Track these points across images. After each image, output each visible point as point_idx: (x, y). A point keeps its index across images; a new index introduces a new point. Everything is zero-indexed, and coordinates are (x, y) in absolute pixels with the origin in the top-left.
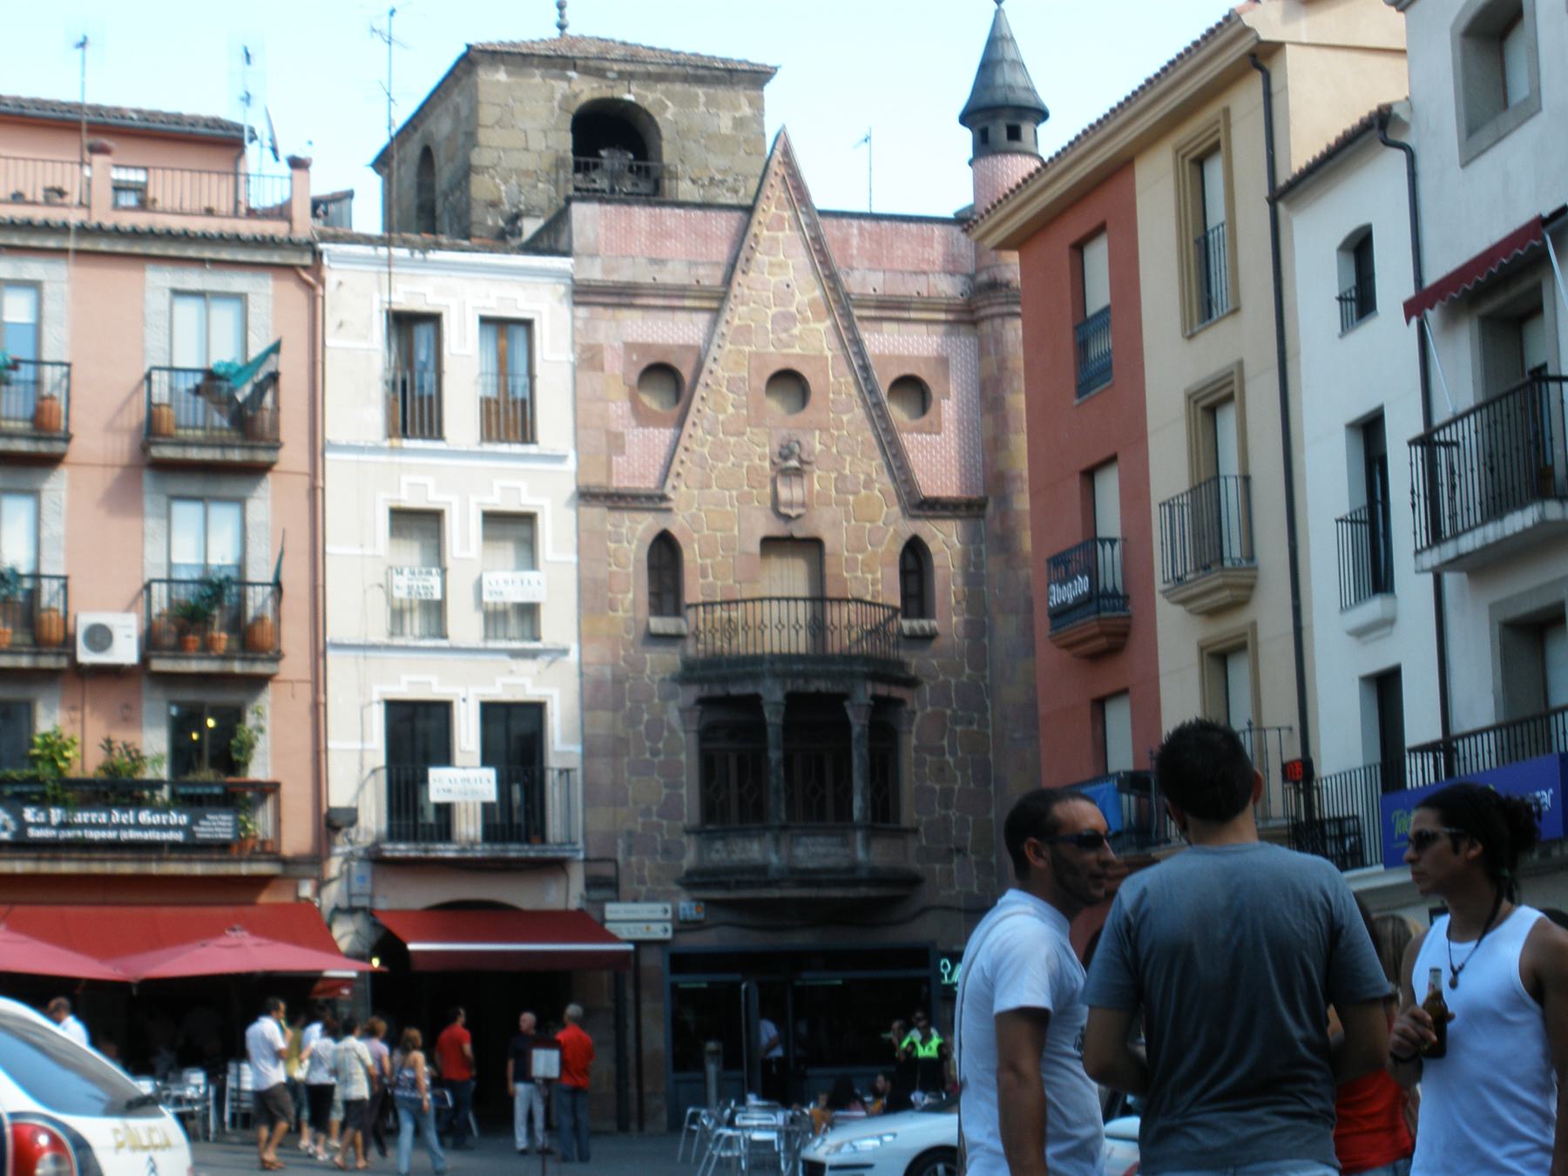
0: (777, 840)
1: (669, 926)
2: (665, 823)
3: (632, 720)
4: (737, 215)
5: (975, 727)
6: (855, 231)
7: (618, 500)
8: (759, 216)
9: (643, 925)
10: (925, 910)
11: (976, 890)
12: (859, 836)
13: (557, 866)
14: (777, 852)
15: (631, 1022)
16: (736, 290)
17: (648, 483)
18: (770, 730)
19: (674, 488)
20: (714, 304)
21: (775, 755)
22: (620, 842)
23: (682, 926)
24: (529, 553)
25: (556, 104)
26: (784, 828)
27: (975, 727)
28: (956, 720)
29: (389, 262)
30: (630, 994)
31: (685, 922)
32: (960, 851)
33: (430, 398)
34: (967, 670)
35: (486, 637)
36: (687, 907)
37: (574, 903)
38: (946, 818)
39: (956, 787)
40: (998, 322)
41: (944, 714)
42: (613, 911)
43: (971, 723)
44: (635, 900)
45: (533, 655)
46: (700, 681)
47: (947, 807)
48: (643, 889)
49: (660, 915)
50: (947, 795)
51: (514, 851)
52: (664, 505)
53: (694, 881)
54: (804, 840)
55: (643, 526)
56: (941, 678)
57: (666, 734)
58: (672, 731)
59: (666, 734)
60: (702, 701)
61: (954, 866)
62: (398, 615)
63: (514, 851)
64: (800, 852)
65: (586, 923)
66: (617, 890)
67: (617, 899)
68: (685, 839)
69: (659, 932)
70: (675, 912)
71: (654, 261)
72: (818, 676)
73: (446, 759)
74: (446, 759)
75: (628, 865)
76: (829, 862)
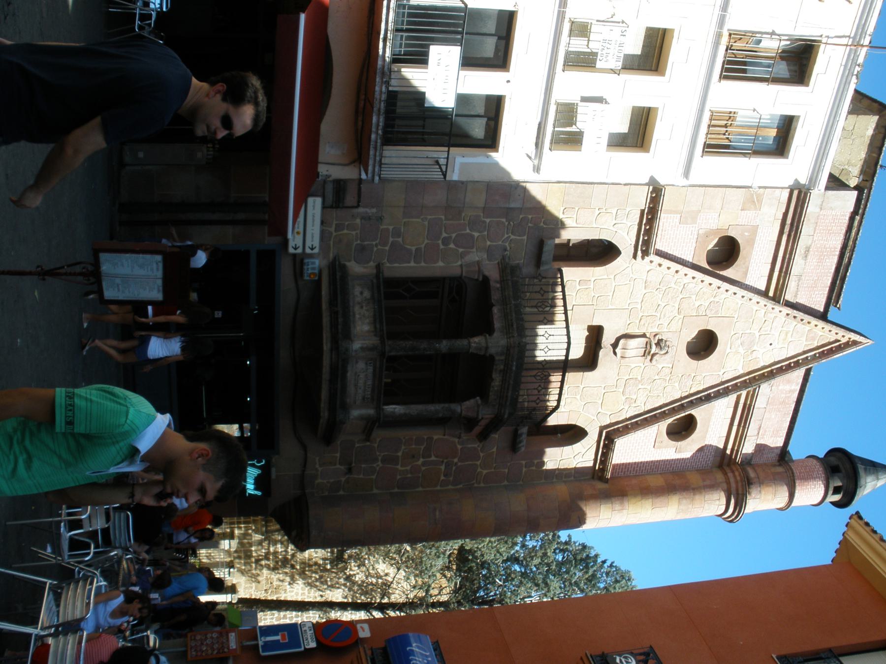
0: (372, 349)
1: (300, 251)
2: (387, 248)
6: (793, 388)
7: (650, 217)
8: (821, 324)
10: (305, 448)
11: (319, 481)
12: (371, 412)
13: (359, 153)
14: (362, 348)
15: (216, 217)
16: (778, 308)
17: (661, 242)
18: (465, 342)
19: (651, 262)
20: (771, 294)
21: (444, 345)
22: (374, 210)
23: (299, 261)
24: (619, 142)
25: (846, 167)
27: (442, 478)
29: (858, 45)
30: (240, 216)
31: (302, 263)
32: (350, 470)
33: (744, 71)
34: (485, 472)
35: (558, 104)
36: (314, 265)
37: (322, 170)
39: (399, 467)
40: (725, 486)
42: (315, 205)
44: (322, 223)
45: (538, 144)
46: (502, 281)
47: (384, 461)
48: (333, 229)
49: (309, 243)
51: (377, 120)
52: (639, 253)
54: (371, 369)
55: (625, 237)
56: (482, 455)
58: (462, 256)
59: (461, 250)
60: (486, 281)
61: (338, 466)
62: (581, 30)
63: (377, 120)
64: (361, 365)
65: (309, 180)
66: (332, 207)
67: (324, 207)
68: (372, 264)
69: (294, 241)
70: (311, 256)
71: (808, 250)
73: (469, 62)
74: (469, 62)
75: (353, 217)
76: (351, 389)
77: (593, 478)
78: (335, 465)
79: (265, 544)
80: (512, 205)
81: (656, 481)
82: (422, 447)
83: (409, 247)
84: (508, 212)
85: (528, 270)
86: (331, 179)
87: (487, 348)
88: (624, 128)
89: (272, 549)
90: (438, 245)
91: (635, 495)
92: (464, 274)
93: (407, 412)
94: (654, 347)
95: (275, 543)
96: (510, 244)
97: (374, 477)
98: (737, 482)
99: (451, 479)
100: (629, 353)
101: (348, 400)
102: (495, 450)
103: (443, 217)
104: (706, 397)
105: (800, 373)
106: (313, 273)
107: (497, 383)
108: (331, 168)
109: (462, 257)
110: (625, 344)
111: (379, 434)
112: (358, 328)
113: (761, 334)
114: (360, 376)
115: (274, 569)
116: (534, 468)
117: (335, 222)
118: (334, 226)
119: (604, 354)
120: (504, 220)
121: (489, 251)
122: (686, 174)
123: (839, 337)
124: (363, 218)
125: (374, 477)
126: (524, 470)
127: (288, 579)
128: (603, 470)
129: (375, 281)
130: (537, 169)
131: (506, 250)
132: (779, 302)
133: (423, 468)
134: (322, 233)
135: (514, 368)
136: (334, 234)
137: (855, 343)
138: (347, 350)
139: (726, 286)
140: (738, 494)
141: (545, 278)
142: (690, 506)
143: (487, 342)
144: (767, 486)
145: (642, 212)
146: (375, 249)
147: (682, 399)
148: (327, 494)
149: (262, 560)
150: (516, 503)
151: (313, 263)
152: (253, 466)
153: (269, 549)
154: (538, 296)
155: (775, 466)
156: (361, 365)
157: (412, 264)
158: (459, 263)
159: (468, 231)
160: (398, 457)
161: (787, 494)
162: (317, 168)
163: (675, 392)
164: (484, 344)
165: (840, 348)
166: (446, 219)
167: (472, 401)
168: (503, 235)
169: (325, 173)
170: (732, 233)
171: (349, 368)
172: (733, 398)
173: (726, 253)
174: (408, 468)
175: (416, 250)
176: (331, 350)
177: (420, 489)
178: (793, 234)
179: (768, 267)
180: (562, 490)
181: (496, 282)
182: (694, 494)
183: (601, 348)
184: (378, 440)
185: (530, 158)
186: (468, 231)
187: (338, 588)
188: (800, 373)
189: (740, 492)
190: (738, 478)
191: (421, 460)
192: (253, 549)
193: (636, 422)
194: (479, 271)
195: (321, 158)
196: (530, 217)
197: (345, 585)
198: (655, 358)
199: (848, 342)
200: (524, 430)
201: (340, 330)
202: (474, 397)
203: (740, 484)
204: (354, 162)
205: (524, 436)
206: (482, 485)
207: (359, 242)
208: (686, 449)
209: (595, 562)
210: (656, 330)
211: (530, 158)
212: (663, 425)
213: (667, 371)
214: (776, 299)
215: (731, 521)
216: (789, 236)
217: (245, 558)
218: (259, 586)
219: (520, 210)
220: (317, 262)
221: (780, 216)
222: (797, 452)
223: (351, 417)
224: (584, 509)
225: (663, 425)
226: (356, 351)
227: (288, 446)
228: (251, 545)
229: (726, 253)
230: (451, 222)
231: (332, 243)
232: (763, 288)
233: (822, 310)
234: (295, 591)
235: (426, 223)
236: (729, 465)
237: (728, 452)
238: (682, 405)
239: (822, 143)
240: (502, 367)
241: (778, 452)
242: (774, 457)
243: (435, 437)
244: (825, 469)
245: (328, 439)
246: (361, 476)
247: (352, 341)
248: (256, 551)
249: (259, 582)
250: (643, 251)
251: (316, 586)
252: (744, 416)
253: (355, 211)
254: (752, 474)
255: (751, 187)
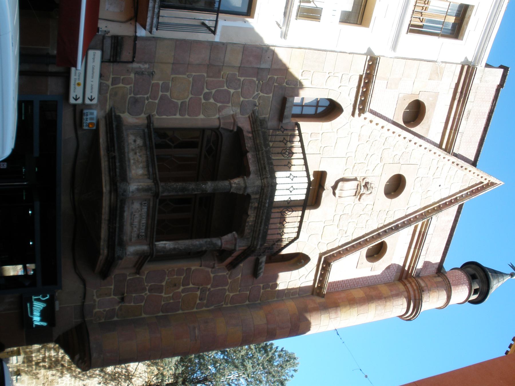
0: (146, 190)
1: (80, 101)
2: (157, 101)
3: (231, 81)
4: (472, 158)
5: (198, 301)
7: (367, 81)
9: (82, 81)
12: (145, 248)
14: (138, 190)
17: (374, 104)
18: (226, 183)
19: (365, 119)
21: (209, 186)
22: (147, 66)
23: (79, 112)
26: (156, 195)
27: (198, 301)
28: (203, 291)
31: (82, 114)
32: (123, 300)
34: (231, 294)
36: (93, 116)
37: (102, 25)
38: (144, 289)
39: (163, 295)
40: (406, 294)
41: (208, 284)
43: (201, 299)
44: (101, 76)
45: (286, 14)
47: (150, 290)
48: (109, 83)
49: (88, 95)
50: (160, 289)
52: (357, 111)
53: (112, 121)
55: (346, 100)
56: (229, 281)
57: (219, 105)
58: (220, 110)
59: (219, 105)
60: (240, 130)
61: (112, 297)
64: (136, 206)
66: (109, 61)
67: (103, 61)
68: (143, 116)
69: (75, 92)
70: (89, 107)
72: (257, 216)
76: (127, 228)
77: (312, 294)
78: (110, 295)
79: (42, 351)
80: (263, 66)
81: (358, 294)
82: (182, 277)
83: (176, 101)
84: (258, 72)
85: (272, 123)
86: (109, 35)
87: (246, 188)
88: (349, 8)
89: (47, 354)
90: (200, 99)
91: (345, 306)
92: (222, 126)
93: (176, 247)
94: (362, 188)
95: (50, 349)
96: (259, 100)
97: (143, 304)
98: (414, 291)
99: (205, 302)
100: (344, 194)
101: (125, 238)
102: (240, 276)
103: (205, 75)
104: (395, 228)
105: (454, 209)
106: (91, 123)
107: (252, 219)
108: (109, 24)
109: (219, 111)
110: (342, 186)
111: (148, 267)
112: (133, 172)
113: (435, 177)
114: (136, 216)
115: (50, 368)
116: (269, 289)
117: (112, 76)
118: (111, 80)
119: (326, 195)
120: (255, 79)
121: (242, 106)
122: (394, 47)
123: (482, 180)
124: (136, 73)
125: (143, 304)
126: (262, 291)
127: (59, 374)
128: (321, 288)
129: (146, 130)
130: (284, 35)
131: (255, 105)
132: (449, 153)
133: (183, 295)
134: (101, 85)
135: (267, 205)
136: (111, 87)
137: (493, 184)
138: (125, 191)
139: (416, 139)
140: (415, 299)
141: (287, 130)
142: (383, 311)
143: (245, 183)
144: (433, 292)
145: (361, 77)
146: (146, 102)
147: (379, 229)
148: (103, 320)
149: (40, 362)
150: (258, 318)
151: (92, 114)
152: (38, 300)
153: (45, 354)
154: (282, 144)
155: (435, 277)
156: (136, 206)
157: (178, 116)
158: (217, 116)
159: (226, 88)
160: (162, 286)
161: (446, 297)
162: (97, 23)
163: (374, 224)
164: (242, 184)
165: (483, 188)
166: (208, 77)
167: (230, 235)
168: (254, 93)
169: (104, 29)
170: (421, 99)
171: (126, 209)
172: (412, 228)
173: (416, 113)
174: (171, 295)
175: (182, 103)
176: (110, 192)
177: (180, 312)
178: (462, 100)
179: (443, 125)
180: (290, 306)
181: (249, 132)
182: (386, 302)
183: (324, 189)
184: (146, 272)
185: (279, 25)
186: (226, 88)
187: (95, 377)
188: (454, 209)
189: (417, 298)
190: (415, 288)
191: (182, 288)
192: (33, 355)
193: (346, 249)
194: (235, 123)
195: (101, 15)
196: (276, 77)
197: (100, 375)
198: (363, 197)
199: (488, 184)
200: (263, 259)
201: (118, 174)
202: (231, 232)
203: (417, 292)
204: (131, 19)
205: (263, 264)
206: (229, 305)
207: (132, 95)
208: (378, 268)
209: (271, 348)
210: (364, 175)
211: (279, 25)
212: (364, 251)
213: (370, 207)
214: (448, 150)
215: (409, 320)
216: (459, 101)
217: (27, 363)
218: (39, 381)
219: (268, 70)
220: (95, 112)
221: (453, 86)
222: (447, 267)
223: (128, 253)
224: (309, 319)
225: (364, 251)
226: (133, 192)
227: (70, 282)
228: (32, 352)
229: (416, 113)
230: (211, 79)
231: (108, 95)
232: (438, 142)
233: (473, 160)
234: (65, 382)
235: (191, 79)
236: (406, 278)
237: (406, 268)
238: (379, 234)
239: (486, 30)
240: (256, 205)
241: (437, 266)
242: (434, 270)
243: (193, 268)
244: (468, 277)
245: (104, 274)
246: (132, 304)
247: (129, 184)
248: (35, 356)
249: (38, 379)
250: (360, 110)
251: (80, 378)
252: (419, 241)
253: (130, 66)
254: (423, 284)
255: (436, 62)
